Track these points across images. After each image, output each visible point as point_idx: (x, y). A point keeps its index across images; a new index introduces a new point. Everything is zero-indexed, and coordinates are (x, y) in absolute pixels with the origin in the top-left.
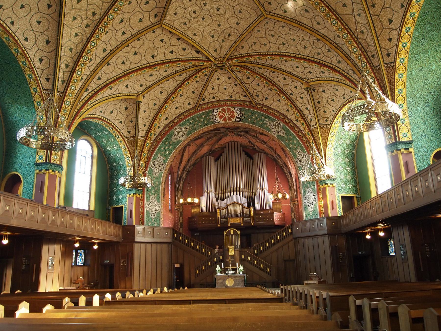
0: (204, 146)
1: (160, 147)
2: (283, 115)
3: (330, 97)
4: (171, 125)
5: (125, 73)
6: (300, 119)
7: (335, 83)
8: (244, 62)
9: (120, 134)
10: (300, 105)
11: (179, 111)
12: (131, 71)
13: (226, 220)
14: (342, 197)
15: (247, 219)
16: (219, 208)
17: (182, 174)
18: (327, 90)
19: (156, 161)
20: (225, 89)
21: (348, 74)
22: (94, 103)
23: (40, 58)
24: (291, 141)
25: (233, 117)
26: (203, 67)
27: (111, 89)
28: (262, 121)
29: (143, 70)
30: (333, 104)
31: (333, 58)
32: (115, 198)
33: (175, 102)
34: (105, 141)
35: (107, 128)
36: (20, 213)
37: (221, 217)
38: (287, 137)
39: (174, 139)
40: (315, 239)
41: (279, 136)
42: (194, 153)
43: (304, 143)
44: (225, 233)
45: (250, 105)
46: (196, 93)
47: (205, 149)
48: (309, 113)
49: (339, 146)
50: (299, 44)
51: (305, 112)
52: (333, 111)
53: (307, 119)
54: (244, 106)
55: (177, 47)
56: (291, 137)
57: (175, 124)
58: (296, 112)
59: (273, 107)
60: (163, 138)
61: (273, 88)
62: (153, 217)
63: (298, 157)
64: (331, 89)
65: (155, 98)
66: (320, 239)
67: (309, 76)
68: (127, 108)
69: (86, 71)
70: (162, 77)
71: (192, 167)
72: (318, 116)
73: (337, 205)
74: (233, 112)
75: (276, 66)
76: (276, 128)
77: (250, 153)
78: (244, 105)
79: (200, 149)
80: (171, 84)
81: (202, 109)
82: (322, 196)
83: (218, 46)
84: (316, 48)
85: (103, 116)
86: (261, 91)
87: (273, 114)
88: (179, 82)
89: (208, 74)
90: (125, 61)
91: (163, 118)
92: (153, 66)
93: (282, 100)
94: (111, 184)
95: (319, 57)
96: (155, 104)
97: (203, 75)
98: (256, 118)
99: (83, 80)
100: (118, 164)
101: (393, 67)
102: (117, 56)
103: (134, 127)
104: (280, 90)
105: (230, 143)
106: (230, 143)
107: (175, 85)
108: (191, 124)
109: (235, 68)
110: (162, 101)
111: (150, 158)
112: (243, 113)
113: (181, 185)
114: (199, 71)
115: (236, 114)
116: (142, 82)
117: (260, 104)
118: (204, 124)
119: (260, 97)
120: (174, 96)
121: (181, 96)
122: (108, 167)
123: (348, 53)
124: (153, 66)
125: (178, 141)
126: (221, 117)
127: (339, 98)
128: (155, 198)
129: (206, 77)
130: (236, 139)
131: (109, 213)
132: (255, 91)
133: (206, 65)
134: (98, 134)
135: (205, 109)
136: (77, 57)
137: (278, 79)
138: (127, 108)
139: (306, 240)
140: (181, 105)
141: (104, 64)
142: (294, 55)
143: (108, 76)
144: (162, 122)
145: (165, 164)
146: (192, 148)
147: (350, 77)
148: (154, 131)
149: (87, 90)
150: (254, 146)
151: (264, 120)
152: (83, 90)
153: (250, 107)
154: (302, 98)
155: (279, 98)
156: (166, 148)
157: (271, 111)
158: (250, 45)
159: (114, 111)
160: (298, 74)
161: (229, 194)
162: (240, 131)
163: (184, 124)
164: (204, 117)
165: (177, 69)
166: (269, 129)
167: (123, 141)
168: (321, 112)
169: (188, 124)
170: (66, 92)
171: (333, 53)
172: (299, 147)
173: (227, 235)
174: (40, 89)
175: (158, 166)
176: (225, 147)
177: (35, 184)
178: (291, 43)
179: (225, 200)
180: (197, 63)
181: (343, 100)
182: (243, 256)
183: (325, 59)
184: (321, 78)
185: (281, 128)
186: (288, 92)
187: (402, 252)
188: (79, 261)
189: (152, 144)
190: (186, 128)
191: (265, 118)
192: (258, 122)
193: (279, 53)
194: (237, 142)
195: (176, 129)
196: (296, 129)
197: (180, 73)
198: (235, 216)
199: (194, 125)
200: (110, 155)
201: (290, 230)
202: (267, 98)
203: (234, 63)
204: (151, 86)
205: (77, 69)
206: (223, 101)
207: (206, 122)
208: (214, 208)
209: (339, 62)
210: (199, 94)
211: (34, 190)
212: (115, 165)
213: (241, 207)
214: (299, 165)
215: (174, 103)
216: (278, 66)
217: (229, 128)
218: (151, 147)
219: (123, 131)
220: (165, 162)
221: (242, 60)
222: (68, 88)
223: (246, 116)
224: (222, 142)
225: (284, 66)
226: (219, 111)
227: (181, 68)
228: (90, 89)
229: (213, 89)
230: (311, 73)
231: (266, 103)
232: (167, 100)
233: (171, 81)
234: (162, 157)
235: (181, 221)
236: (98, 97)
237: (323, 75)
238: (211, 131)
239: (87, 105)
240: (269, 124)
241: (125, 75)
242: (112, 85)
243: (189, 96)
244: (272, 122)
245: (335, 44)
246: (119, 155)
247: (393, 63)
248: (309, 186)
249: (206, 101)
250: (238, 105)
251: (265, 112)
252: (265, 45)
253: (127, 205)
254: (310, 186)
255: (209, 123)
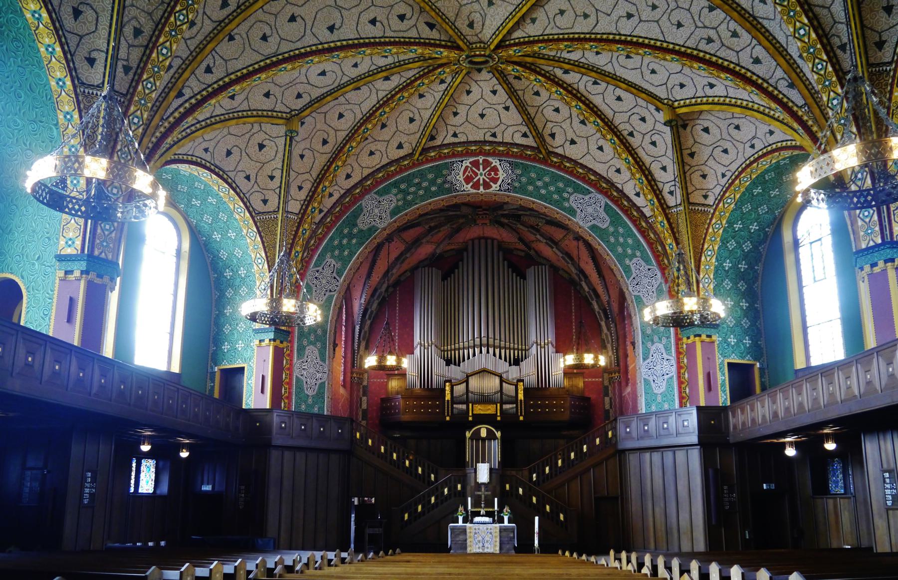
0: (422, 243)
1: (332, 239)
2: (608, 181)
3: (718, 144)
4: (358, 191)
5: (268, 61)
6: (646, 191)
7: (738, 110)
8: (534, 55)
9: (245, 204)
10: (647, 160)
11: (376, 162)
12: (280, 57)
13: (464, 407)
14: (729, 364)
15: (511, 406)
16: (450, 381)
17: (368, 304)
18: (715, 127)
19: (320, 269)
20: (482, 116)
21: (776, 88)
22: (193, 128)
23: (76, 6)
24: (621, 240)
25: (495, 180)
26: (440, 62)
27: (232, 98)
28: (559, 191)
29: (307, 59)
30: (725, 159)
31: (745, 50)
32: (226, 347)
33: (370, 140)
34: (207, 218)
35: (216, 188)
36: (27, 364)
37: (454, 400)
38: (612, 229)
39: (363, 223)
40: (669, 455)
41: (594, 228)
42: (397, 259)
43: (650, 245)
44: (468, 434)
45: (539, 153)
46: (416, 124)
47: (425, 250)
48: (667, 178)
49: (726, 254)
50: (666, 16)
51: (658, 174)
52: (724, 175)
53: (661, 192)
54: (521, 157)
55: (386, 11)
56: (621, 230)
57: (366, 190)
58: (638, 176)
59: (587, 162)
60: (338, 218)
61: (592, 119)
62: (310, 393)
63: (634, 275)
64: (723, 125)
65: (325, 127)
66: (680, 455)
67: (678, 94)
68: (264, 146)
69: (180, 48)
70: (345, 79)
71: (391, 290)
72: (688, 184)
73: (720, 382)
74: (495, 169)
75: (605, 68)
76: (590, 210)
77: (519, 263)
78: (521, 155)
79: (413, 250)
80: (384, 87)
81: (427, 160)
82: (685, 361)
83: (478, 15)
84: (705, 27)
85: (209, 159)
86: (563, 125)
87: (584, 177)
88: (381, 94)
89: (449, 80)
90: (268, 33)
91: (342, 173)
92: (330, 50)
93: (608, 147)
94: (217, 315)
95: (711, 48)
96: (325, 142)
97: (438, 81)
98: (546, 185)
99: (172, 71)
100: (235, 272)
101: (888, 73)
102: (252, 20)
103: (277, 191)
104: (606, 124)
105: (476, 242)
106: (476, 242)
107: (373, 101)
108: (400, 191)
109: (510, 68)
110: (342, 135)
111: (308, 263)
112: (519, 172)
113: (366, 328)
114: (430, 72)
115: (501, 175)
116: (300, 88)
117: (557, 155)
118: (429, 194)
119: (559, 140)
120: (370, 126)
121: (384, 126)
122: (212, 279)
123: (782, 39)
124: (330, 50)
125: (370, 229)
126: (468, 180)
127: (740, 147)
128: (317, 352)
129: (444, 86)
130: (492, 232)
131: (213, 381)
132: (549, 125)
133: (447, 57)
134: (194, 202)
135: (433, 160)
136: (160, 13)
137: (603, 96)
138: (264, 146)
139: (647, 455)
140: (381, 146)
141: (221, 36)
142: (652, 42)
143: (229, 67)
144: (339, 185)
145: (340, 277)
146: (396, 248)
147: (781, 96)
148: (320, 203)
149: (180, 94)
150: (530, 249)
151: (564, 191)
152: (173, 94)
153: (534, 160)
154: (654, 143)
155: (602, 142)
156: (345, 242)
157: (580, 171)
158: (551, 16)
159: (235, 151)
160: (652, 89)
161: (471, 351)
162: (503, 215)
163: (386, 191)
164: (430, 176)
165: (382, 62)
166: (572, 212)
167: (251, 221)
168: (696, 178)
169: (394, 191)
170: (133, 95)
171: (745, 37)
172: (638, 254)
173: (471, 438)
174: (73, 81)
175: (324, 281)
176: (466, 249)
177: (54, 304)
178: (647, 14)
179: (452, 366)
180: (427, 52)
181: (749, 152)
182: (508, 486)
183: (723, 53)
184: (705, 100)
185: (602, 210)
186: (625, 128)
187: (888, 492)
188: (142, 483)
189: (314, 232)
190: (391, 201)
191: (566, 186)
192: (550, 193)
193: (617, 37)
194: (493, 240)
195: (368, 202)
196: (635, 213)
197: (386, 72)
198: (485, 399)
199: (409, 194)
200: (219, 252)
201: (459, 486)
202: (573, 142)
203: (510, 56)
204: (320, 99)
205: (161, 40)
206: (475, 143)
207: (433, 189)
208: (436, 381)
209: (757, 61)
210: (423, 124)
211: (53, 318)
212: (228, 274)
213: (497, 380)
214: (636, 293)
215: (366, 142)
216: (609, 68)
217: (480, 207)
218: (310, 238)
219: (252, 199)
220: (340, 274)
221: (528, 49)
222: (137, 85)
223: (524, 179)
224: (463, 237)
225: (622, 69)
226: (464, 165)
227: (390, 60)
228: (188, 93)
229: (455, 114)
230: (682, 86)
231: (572, 152)
232: (353, 134)
233: (365, 89)
234: (334, 262)
235: (364, 406)
236: (202, 114)
237: (709, 92)
238: (441, 210)
239: (179, 129)
240: (574, 200)
241: (267, 68)
242: (237, 88)
243: (400, 128)
244: (581, 196)
245: (751, 19)
246: (238, 253)
247: (890, 63)
248: (656, 339)
249: (438, 142)
250: (508, 153)
251: (567, 172)
252: (586, 16)
253: (254, 363)
254: (660, 339)
255: (441, 190)
